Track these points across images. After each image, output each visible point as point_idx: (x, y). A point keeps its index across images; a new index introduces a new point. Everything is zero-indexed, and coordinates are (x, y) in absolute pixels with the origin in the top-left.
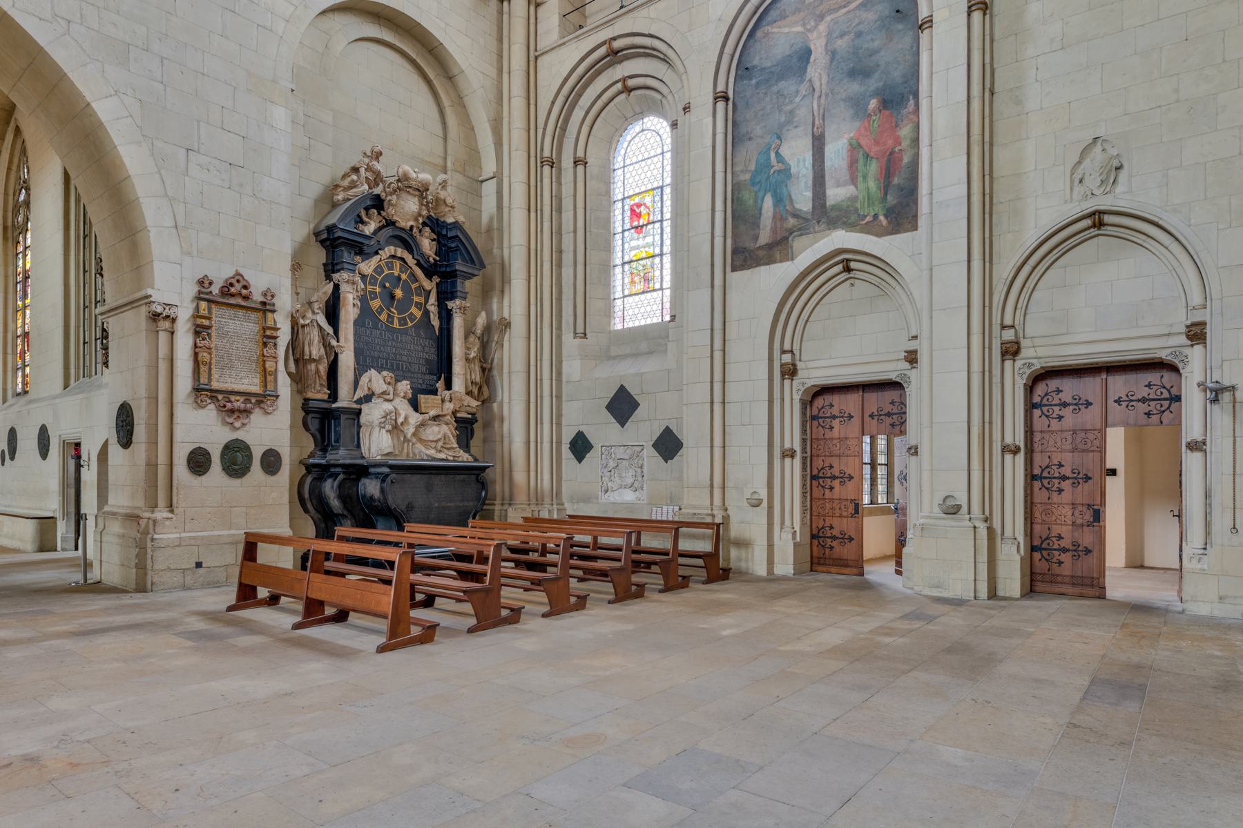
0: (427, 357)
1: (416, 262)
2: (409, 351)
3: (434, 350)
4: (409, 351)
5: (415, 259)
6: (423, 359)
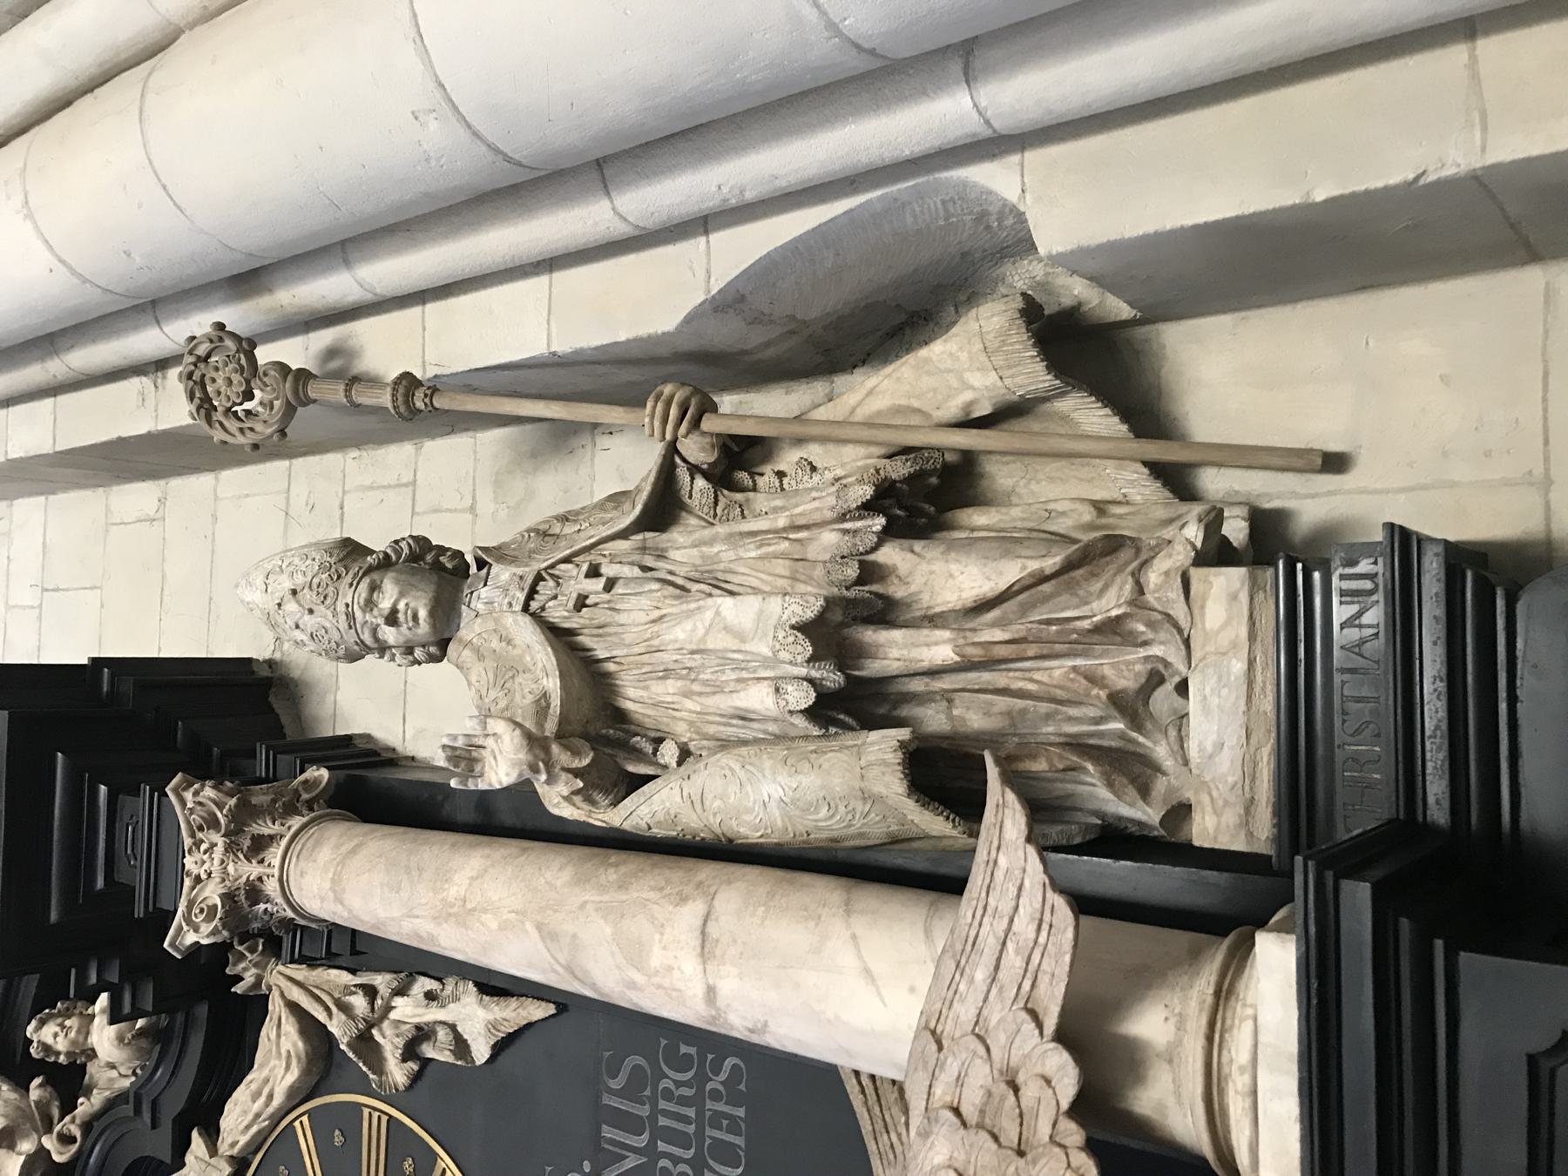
1: (197, 1143)
3: (671, 1077)
5: (183, 1145)
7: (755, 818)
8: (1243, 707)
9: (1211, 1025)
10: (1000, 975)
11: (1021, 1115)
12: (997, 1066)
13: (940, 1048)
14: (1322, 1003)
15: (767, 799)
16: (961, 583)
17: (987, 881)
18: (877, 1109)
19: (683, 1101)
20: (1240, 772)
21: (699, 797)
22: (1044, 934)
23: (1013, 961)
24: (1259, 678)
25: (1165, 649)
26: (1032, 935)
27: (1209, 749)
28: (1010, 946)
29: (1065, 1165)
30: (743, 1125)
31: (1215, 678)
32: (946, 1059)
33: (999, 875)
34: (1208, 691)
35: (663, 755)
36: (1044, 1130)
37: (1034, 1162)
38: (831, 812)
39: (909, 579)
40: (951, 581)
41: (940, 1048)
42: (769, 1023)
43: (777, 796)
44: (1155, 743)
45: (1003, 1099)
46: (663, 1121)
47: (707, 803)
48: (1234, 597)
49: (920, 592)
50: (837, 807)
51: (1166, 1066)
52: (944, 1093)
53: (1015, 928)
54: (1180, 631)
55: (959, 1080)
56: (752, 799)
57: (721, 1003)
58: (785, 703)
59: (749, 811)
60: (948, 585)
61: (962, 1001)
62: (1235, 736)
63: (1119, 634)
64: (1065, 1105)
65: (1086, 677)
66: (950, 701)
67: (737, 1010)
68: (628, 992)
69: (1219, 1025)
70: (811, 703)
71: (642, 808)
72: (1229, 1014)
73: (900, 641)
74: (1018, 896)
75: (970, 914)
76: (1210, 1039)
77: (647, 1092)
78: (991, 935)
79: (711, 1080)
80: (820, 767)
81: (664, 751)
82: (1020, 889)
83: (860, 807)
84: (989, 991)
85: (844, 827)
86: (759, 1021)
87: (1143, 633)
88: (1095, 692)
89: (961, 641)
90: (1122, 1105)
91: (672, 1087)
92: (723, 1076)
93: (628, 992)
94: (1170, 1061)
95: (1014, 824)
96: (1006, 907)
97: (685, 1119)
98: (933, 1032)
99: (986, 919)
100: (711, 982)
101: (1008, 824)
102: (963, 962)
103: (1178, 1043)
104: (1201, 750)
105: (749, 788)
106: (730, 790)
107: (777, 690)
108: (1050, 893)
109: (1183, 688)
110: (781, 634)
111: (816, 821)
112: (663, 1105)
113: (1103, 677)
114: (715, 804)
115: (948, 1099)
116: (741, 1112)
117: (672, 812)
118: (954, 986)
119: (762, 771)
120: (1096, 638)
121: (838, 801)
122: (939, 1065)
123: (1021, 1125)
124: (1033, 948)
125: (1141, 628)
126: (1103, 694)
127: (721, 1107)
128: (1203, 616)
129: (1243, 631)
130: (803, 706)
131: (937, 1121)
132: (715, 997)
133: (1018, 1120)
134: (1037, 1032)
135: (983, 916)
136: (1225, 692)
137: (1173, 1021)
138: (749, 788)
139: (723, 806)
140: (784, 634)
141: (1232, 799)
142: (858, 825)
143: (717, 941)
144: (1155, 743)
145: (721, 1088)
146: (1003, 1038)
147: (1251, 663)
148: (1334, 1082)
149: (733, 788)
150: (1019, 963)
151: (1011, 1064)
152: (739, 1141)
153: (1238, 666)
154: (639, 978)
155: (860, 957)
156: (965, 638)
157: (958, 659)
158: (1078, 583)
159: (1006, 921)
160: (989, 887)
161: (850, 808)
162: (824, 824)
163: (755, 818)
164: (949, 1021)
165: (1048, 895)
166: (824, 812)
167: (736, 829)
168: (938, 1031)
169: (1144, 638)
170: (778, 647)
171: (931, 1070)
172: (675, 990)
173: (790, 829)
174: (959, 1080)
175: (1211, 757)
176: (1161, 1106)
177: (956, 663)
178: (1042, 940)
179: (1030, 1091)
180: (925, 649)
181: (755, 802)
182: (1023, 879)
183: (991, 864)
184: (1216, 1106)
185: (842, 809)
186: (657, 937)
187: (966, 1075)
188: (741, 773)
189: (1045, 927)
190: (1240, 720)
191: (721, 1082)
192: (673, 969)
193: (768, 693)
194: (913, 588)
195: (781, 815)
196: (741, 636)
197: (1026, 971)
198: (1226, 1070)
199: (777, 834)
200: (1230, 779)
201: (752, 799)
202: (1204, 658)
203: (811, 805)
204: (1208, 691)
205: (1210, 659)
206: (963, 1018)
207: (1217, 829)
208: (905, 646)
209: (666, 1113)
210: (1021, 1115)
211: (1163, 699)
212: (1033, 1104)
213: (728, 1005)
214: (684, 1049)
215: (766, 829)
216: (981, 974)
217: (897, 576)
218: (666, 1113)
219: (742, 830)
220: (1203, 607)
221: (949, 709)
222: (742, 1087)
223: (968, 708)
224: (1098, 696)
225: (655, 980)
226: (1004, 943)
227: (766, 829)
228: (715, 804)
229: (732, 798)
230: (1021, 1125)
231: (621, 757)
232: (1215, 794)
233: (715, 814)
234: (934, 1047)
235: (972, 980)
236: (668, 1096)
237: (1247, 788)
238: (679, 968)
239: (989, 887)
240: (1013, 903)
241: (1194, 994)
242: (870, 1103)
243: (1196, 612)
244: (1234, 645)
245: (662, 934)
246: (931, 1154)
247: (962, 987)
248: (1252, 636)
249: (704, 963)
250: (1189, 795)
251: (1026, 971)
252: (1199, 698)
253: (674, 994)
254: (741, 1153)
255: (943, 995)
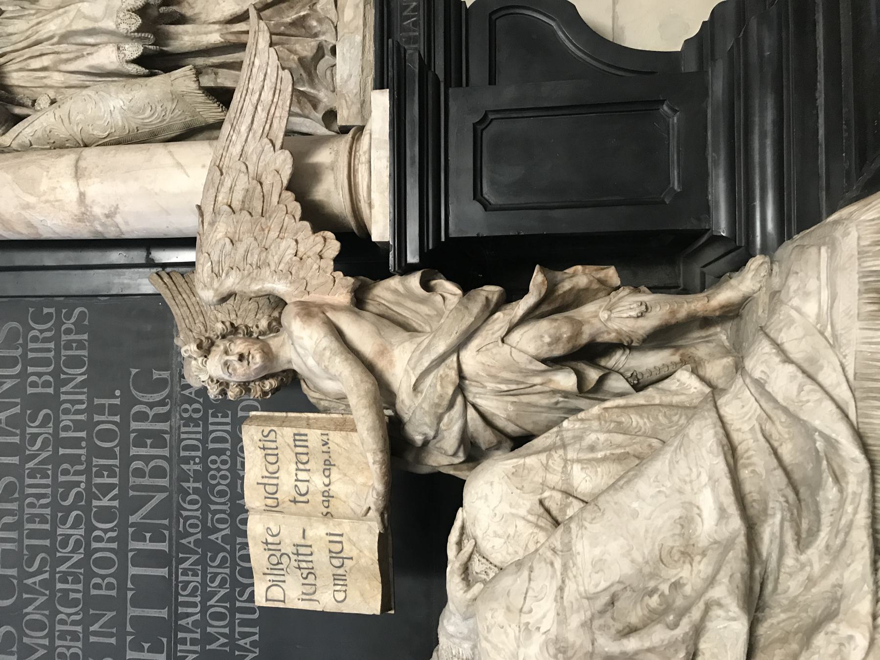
0: (79, 375)
2: (60, 513)
4: (60, 513)
6: (93, 409)
7: (105, 121)
8: (360, 57)
9: (351, 148)
10: (254, 126)
11: (263, 196)
12: (251, 175)
13: (222, 174)
14: (399, 99)
15: (112, 109)
16: (224, 7)
17: (249, 74)
18: (174, 288)
19: (46, 340)
20: (359, 88)
21: (67, 117)
22: (277, 96)
23: (261, 115)
24: (367, 45)
25: (328, 38)
26: (271, 98)
27: (345, 77)
28: (259, 108)
29: (285, 212)
30: (86, 343)
31: (348, 44)
32: (225, 178)
33: (255, 70)
34: (345, 50)
35: (39, 104)
36: (275, 199)
37: (270, 217)
38: (152, 112)
39: (194, 5)
40: (218, 6)
41: (222, 174)
42: (119, 206)
43: (118, 106)
44: (319, 91)
45: (254, 189)
46: (31, 355)
47: (72, 118)
48: (357, 6)
49: (200, 13)
50: (156, 108)
51: (330, 172)
52: (223, 199)
53: (262, 98)
54: (333, 23)
55: (231, 190)
56: (103, 110)
57: (88, 201)
58: (123, 55)
59: (100, 118)
60: (216, 9)
61: (234, 145)
62: (357, 70)
63: (304, 27)
64: (285, 183)
65: (288, 50)
66: (216, 74)
67: (99, 203)
68: (23, 212)
69: (354, 149)
70: (140, 53)
71: (26, 129)
72: (358, 146)
73: (190, 31)
74: (264, 80)
75: (239, 96)
76: (350, 153)
77: (21, 341)
78: (250, 104)
79: (65, 323)
80: (146, 85)
81: (40, 102)
82: (265, 76)
83: (170, 106)
84: (248, 136)
85: (160, 122)
86: (113, 206)
87: (315, 27)
88: (292, 56)
89: (225, 31)
90: (310, 198)
91: (38, 334)
92: (73, 320)
93: (23, 212)
94: (333, 169)
95: (263, 39)
96: (257, 87)
97: (48, 350)
98: (218, 166)
99: (247, 98)
100: (82, 190)
101: (260, 40)
102: (235, 124)
103: (335, 161)
104: (342, 79)
105: (101, 104)
106: (88, 107)
107: (119, 48)
108: (280, 71)
109: (333, 51)
110: (121, 15)
111: (143, 119)
112: (31, 345)
113: (296, 51)
114: (78, 118)
115: (225, 201)
116: (85, 337)
117: (48, 129)
118: (230, 138)
119: (109, 94)
120: (293, 31)
121: (156, 103)
122: (221, 183)
123: (263, 202)
124: (271, 105)
125: (315, 23)
126: (296, 58)
127: (72, 337)
128: (343, 15)
129: (361, 22)
130: (135, 56)
131: (219, 214)
132: (85, 198)
133: (262, 199)
134: (272, 148)
135: (246, 95)
136: (353, 50)
137: (333, 153)
138: (101, 104)
139: (83, 118)
140: (123, 14)
141: (355, 101)
142: (168, 120)
143: (86, 168)
144: (319, 91)
145: (73, 327)
146: (255, 158)
147: (364, 37)
148: (403, 210)
149: (90, 106)
150: (264, 115)
151: (259, 172)
152: (84, 353)
153: (359, 38)
154: (32, 200)
155: (174, 158)
156: (226, 29)
157: (223, 40)
158: (283, 11)
159: (258, 94)
160: (249, 78)
161: (164, 107)
162: (147, 121)
163: (105, 121)
164: (227, 159)
165: (279, 72)
166: (148, 113)
167: (91, 132)
168: (220, 166)
169: (315, 31)
170: (120, 21)
171: (216, 187)
172: (57, 201)
173: (126, 127)
174: (231, 190)
175: (346, 82)
176: (329, 192)
177: (222, 42)
178: (275, 100)
179: (267, 183)
180: (205, 36)
181: (105, 111)
182: (267, 70)
183: (251, 64)
184: (353, 183)
185: (159, 109)
186: (45, 173)
187: (235, 185)
188: (96, 97)
189: (277, 92)
190: (359, 63)
191: (72, 324)
192: (56, 188)
193: (113, 51)
194: (196, 11)
195: (122, 117)
196: (95, 20)
197: (267, 119)
198: (356, 167)
199: (117, 133)
200: (355, 91)
201: (103, 110)
202: (343, 35)
203: (140, 109)
204: (345, 50)
205: (346, 35)
206: (234, 154)
207: (348, 116)
208: (193, 34)
209: (33, 350)
210: (263, 196)
211: (322, 65)
212: (269, 187)
213: (93, 201)
214: (46, 310)
215: (111, 128)
216: (244, 128)
217: (187, 2)
218: (33, 350)
219: (95, 132)
220: (343, 11)
221: (216, 78)
222: (86, 323)
223: (226, 79)
224: (293, 59)
225: (43, 198)
226: (256, 108)
227: (111, 128)
228: (78, 118)
229: (90, 112)
230: (263, 202)
231: (9, 106)
232: (347, 98)
233: (78, 124)
234: (219, 173)
235: (239, 132)
236: (35, 339)
237: (362, 95)
238: (61, 187)
239: (249, 78)
240: (262, 83)
241: (343, 142)
242: (170, 287)
243: (339, 12)
244: (357, 28)
245: (48, 172)
246: (215, 234)
247: (234, 138)
248: (365, 25)
249: (77, 180)
250: (335, 105)
251: (267, 119)
252: (341, 54)
253: (57, 203)
254: (86, 359)
255: (224, 144)
